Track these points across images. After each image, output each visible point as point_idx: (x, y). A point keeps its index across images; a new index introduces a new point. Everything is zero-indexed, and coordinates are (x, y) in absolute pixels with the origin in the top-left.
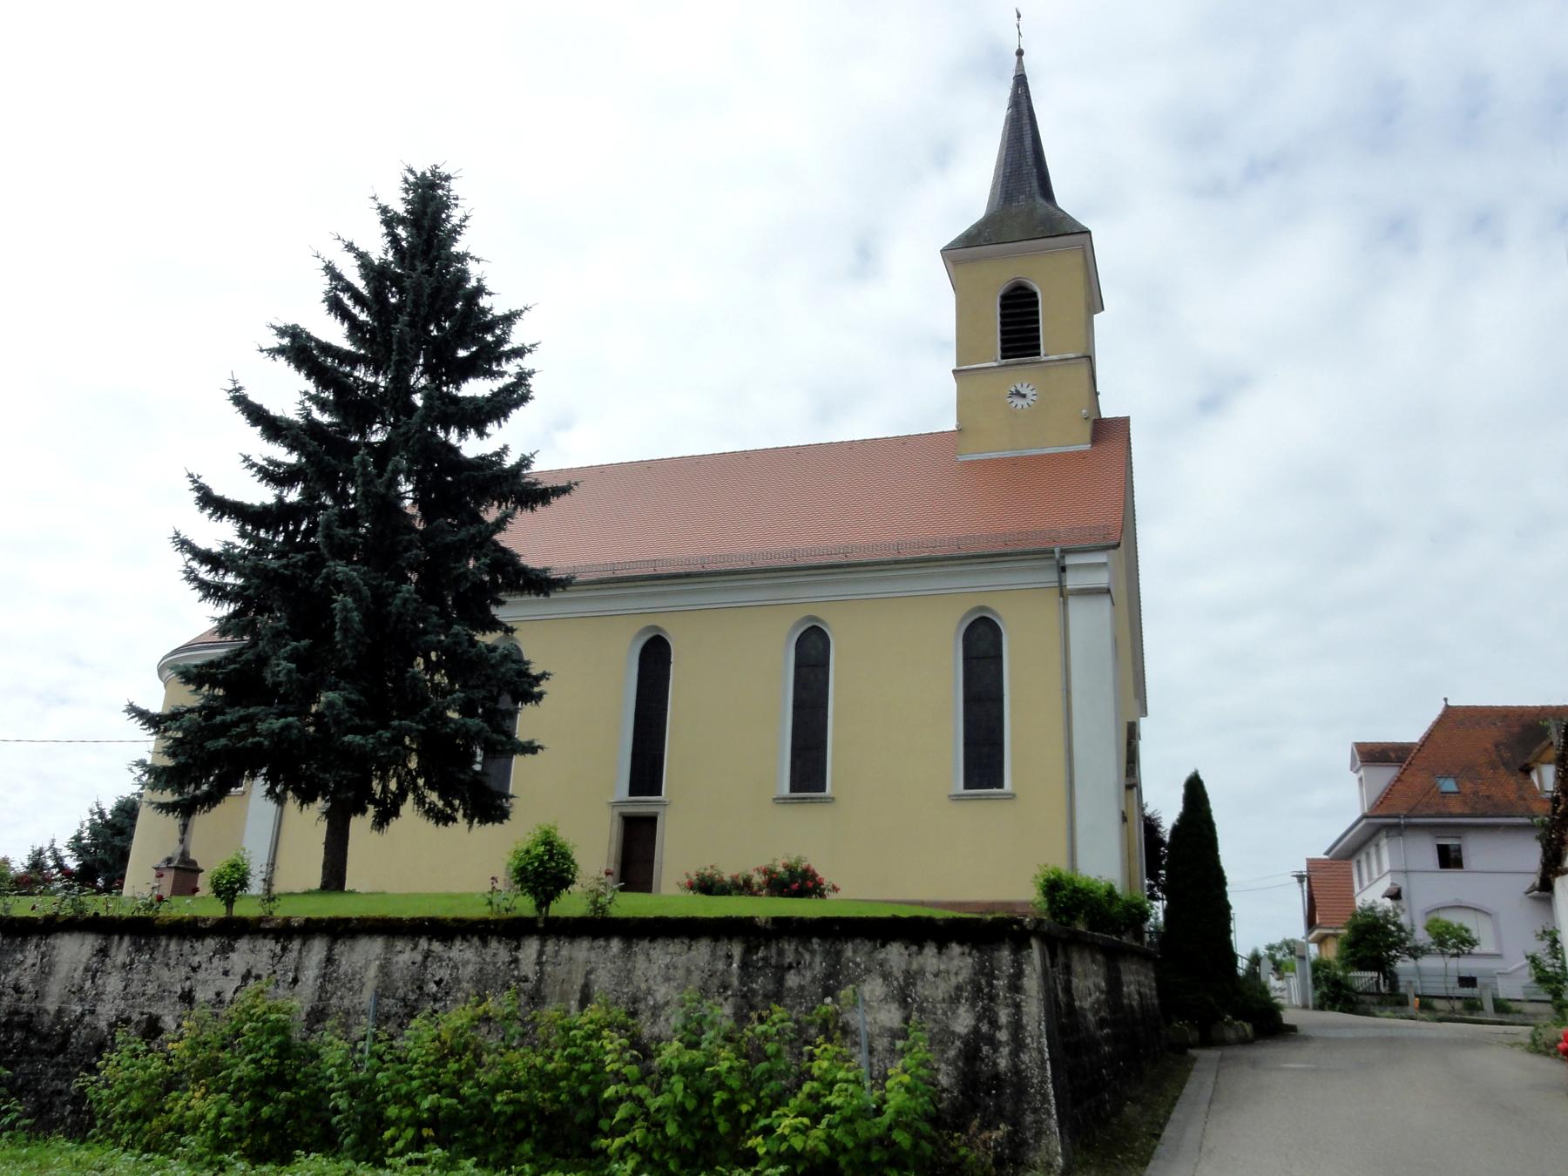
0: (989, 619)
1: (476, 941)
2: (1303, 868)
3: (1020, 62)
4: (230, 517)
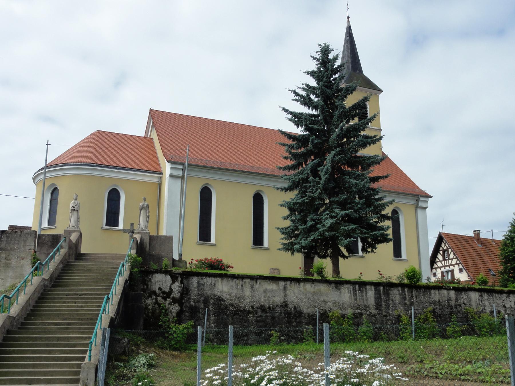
3: (348, 21)
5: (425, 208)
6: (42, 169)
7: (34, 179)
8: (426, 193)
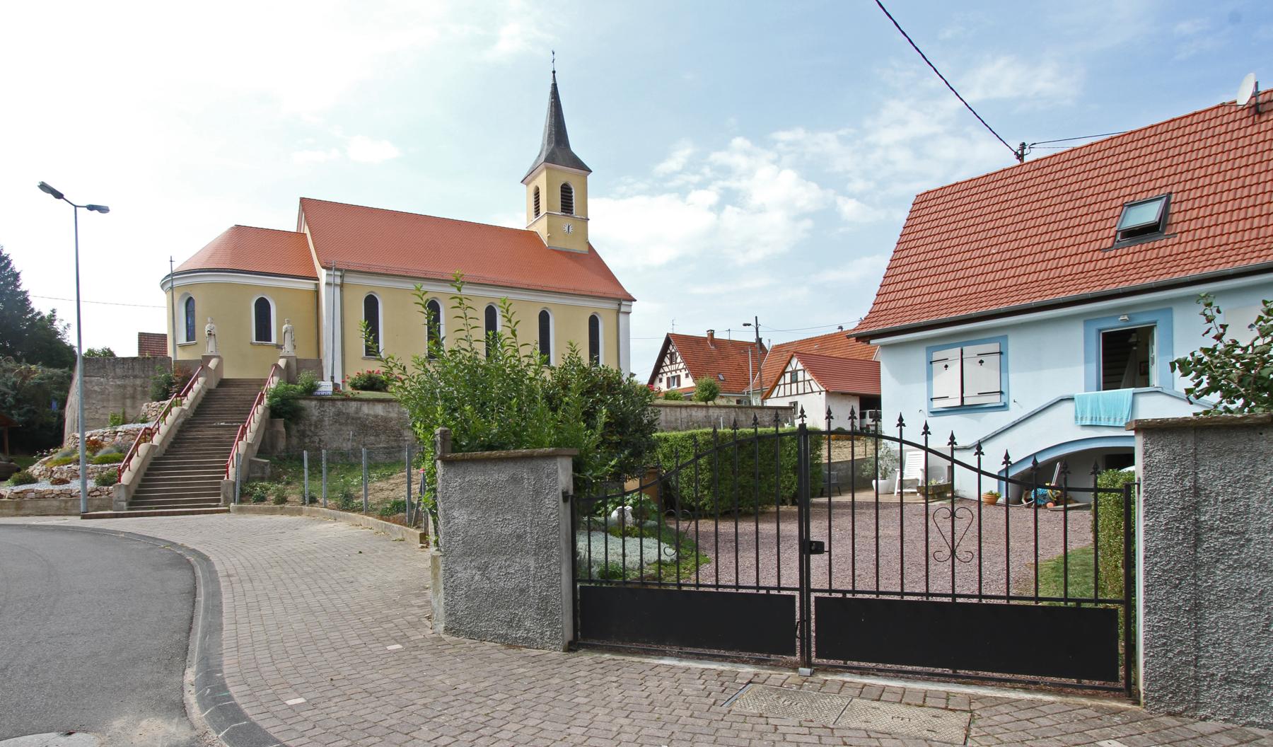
3: (554, 76)
5: (628, 313)
6: (169, 275)
7: (162, 286)
8: (630, 296)
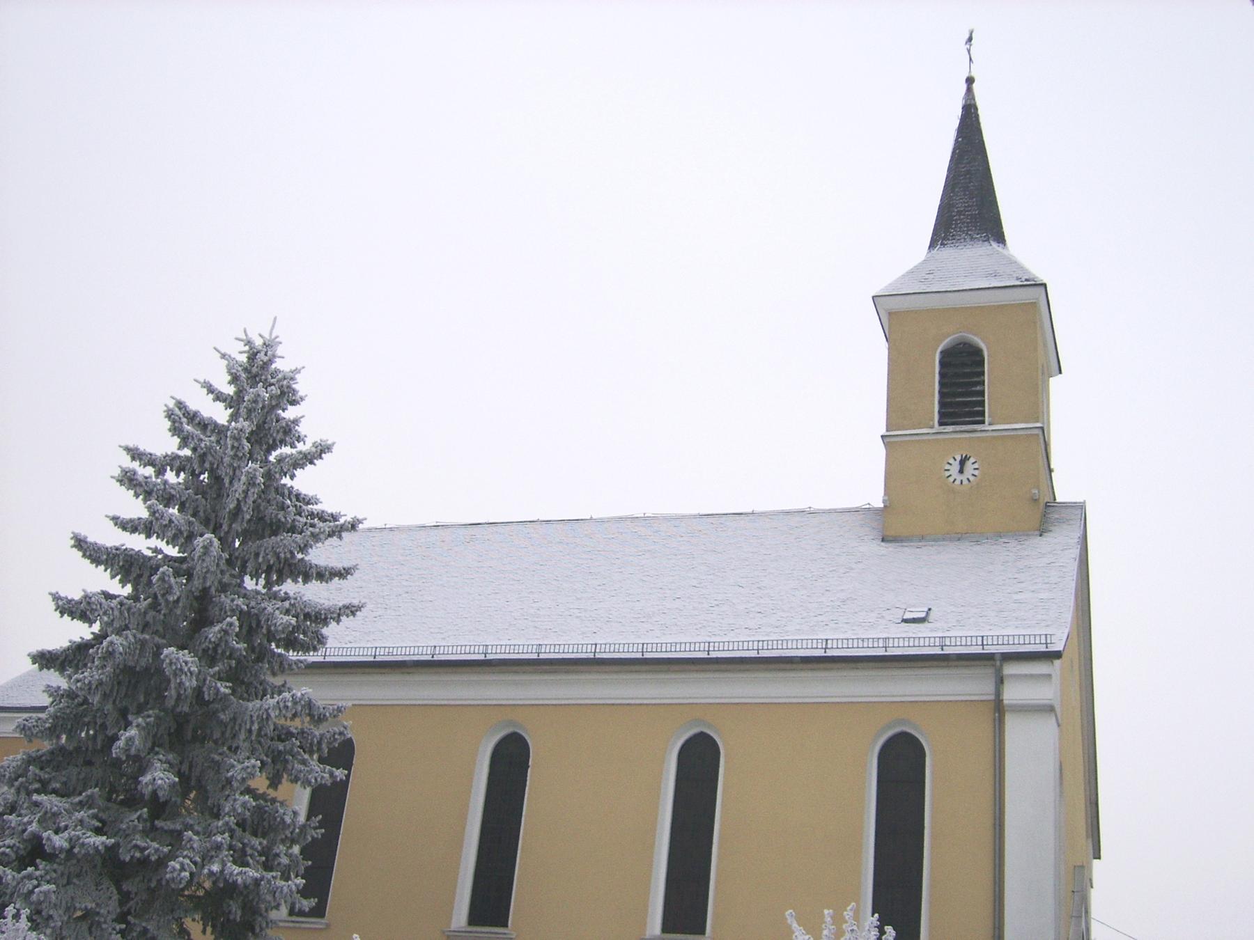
0: (917, 740)
1: (255, 847)
2: (170, 434)
3: (969, 90)
4: (68, 616)
